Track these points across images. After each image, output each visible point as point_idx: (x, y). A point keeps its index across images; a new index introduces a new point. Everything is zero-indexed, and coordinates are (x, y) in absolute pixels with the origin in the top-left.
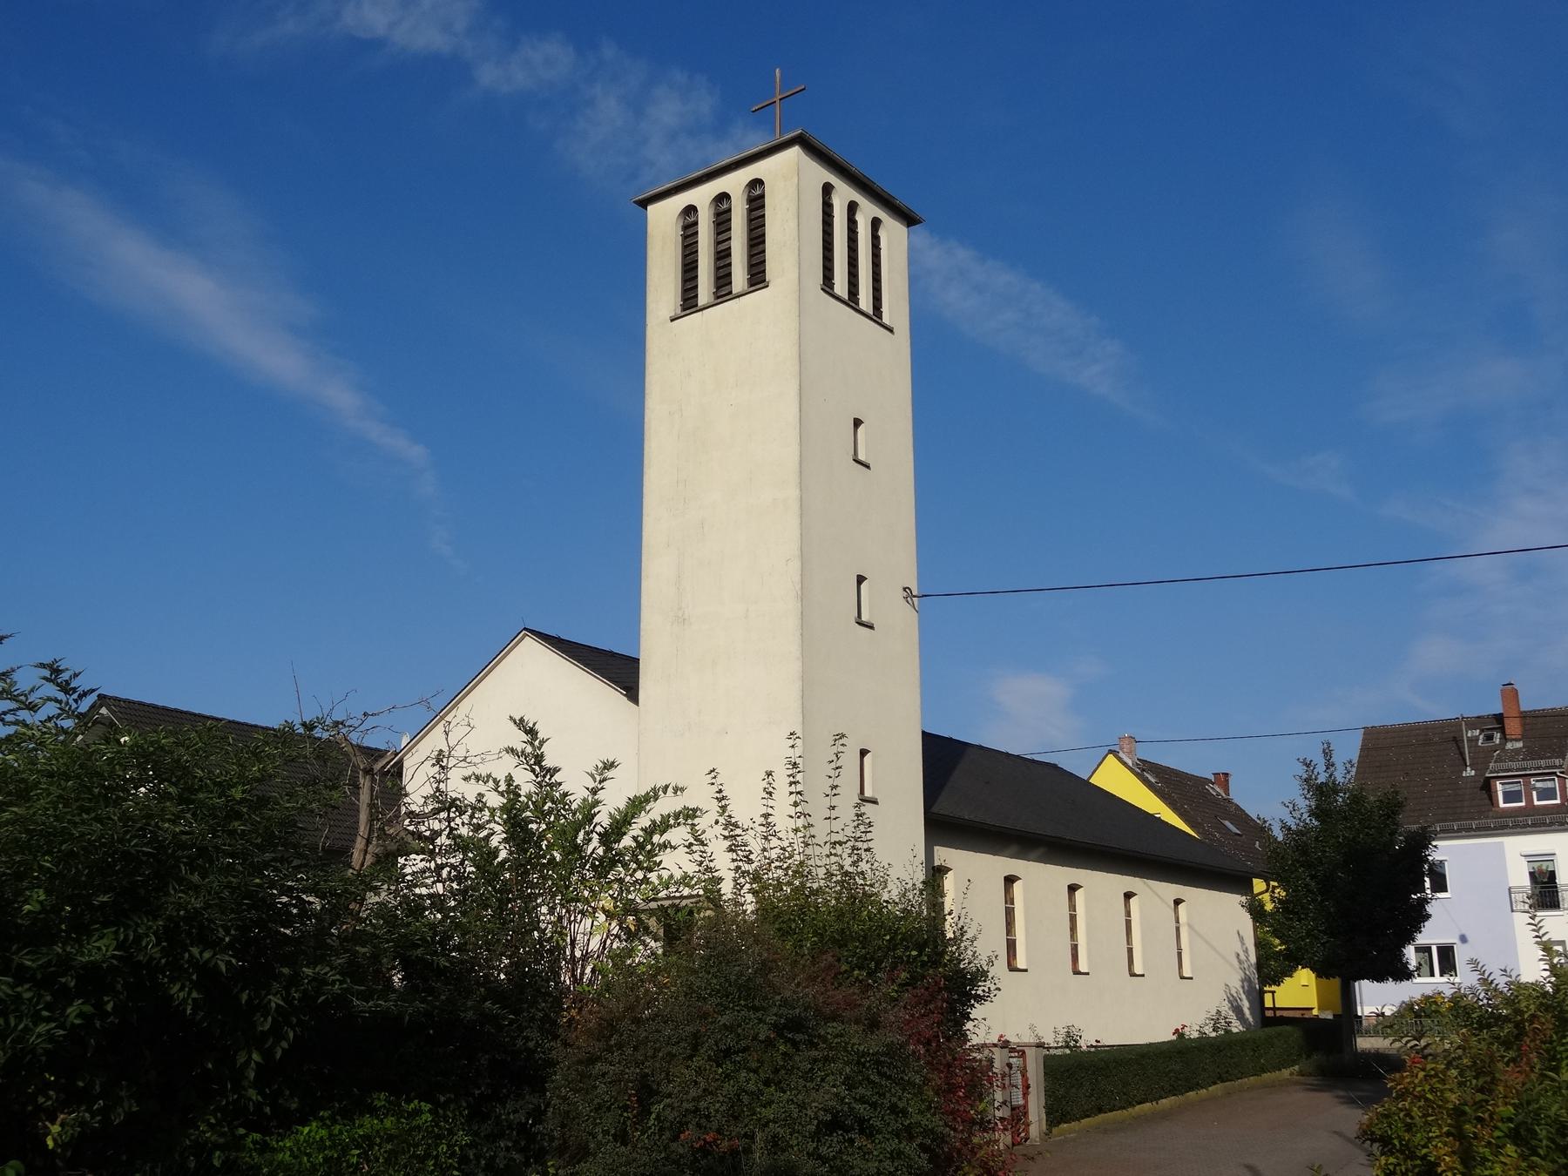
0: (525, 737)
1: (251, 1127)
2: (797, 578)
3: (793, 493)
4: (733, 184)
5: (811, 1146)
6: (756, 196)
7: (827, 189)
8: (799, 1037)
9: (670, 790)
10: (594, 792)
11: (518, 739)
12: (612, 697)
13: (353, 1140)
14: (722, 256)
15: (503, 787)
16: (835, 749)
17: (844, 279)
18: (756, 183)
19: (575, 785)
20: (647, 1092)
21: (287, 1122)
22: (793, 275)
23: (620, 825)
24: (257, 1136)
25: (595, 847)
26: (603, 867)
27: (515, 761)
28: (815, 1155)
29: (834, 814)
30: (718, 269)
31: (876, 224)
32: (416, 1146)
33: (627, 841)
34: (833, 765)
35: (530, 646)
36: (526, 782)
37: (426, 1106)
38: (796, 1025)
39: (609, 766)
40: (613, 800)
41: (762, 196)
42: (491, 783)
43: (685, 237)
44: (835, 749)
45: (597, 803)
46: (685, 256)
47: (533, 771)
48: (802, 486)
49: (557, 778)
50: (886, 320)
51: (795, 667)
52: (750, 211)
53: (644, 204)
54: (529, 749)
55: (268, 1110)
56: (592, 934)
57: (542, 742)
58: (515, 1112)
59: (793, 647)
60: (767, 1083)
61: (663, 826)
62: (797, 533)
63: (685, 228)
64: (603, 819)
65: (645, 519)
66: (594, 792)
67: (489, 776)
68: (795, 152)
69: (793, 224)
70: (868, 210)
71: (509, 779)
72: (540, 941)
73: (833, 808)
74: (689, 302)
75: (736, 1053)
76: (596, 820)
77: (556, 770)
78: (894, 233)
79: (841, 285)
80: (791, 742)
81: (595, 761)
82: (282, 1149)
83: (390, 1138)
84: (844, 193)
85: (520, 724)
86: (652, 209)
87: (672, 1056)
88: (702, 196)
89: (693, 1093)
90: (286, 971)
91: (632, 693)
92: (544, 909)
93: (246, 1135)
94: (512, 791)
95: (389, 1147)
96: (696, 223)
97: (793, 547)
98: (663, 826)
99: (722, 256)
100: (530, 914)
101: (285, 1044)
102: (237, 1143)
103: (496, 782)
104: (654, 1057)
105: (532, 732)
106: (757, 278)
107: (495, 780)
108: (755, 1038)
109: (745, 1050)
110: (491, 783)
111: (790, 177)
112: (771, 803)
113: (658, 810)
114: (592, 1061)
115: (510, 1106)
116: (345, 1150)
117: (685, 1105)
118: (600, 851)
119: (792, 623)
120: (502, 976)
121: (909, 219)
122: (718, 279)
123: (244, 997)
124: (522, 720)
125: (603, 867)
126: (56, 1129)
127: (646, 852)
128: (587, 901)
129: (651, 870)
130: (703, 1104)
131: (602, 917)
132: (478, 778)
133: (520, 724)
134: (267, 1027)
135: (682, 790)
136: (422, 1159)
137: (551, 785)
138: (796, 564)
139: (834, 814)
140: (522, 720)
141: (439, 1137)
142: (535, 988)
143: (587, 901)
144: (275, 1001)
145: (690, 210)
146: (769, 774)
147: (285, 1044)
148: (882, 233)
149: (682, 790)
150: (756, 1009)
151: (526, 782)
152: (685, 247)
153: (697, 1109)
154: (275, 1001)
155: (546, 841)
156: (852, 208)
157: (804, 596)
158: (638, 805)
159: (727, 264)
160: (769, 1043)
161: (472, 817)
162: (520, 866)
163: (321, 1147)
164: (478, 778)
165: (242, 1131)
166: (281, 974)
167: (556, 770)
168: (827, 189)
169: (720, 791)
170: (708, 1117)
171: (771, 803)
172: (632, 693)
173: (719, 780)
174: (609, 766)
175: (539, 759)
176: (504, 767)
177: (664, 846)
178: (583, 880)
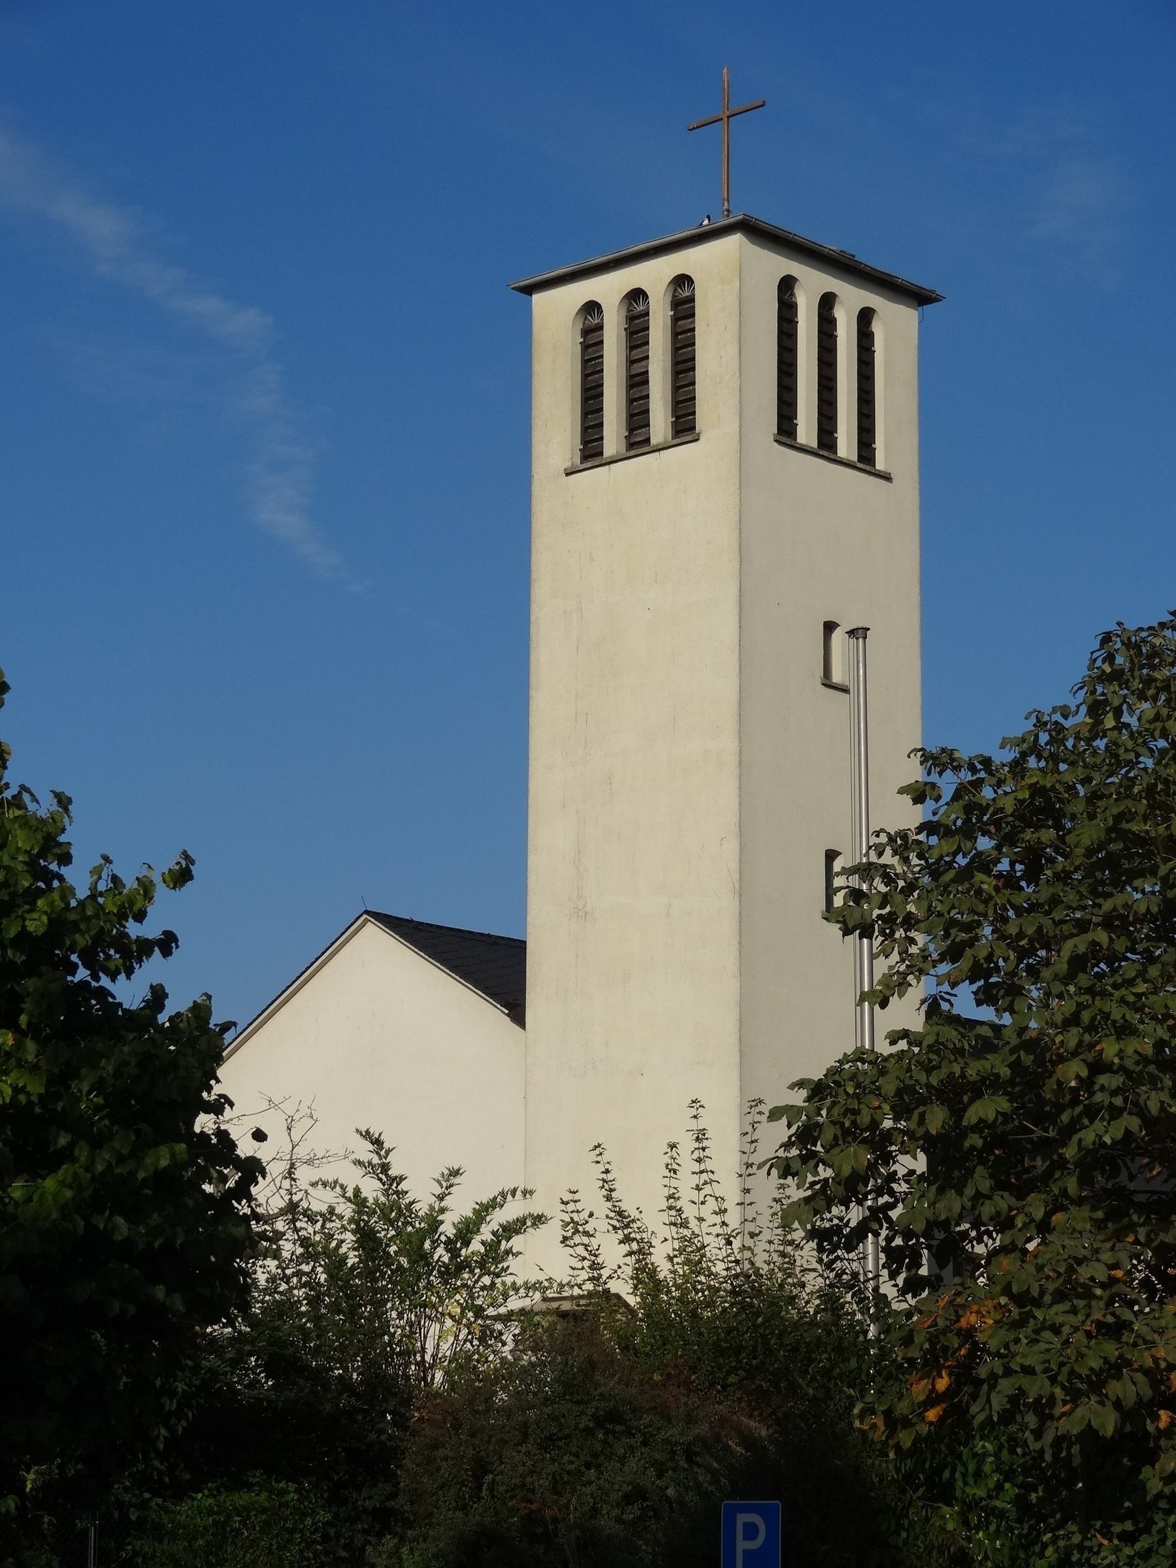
0: (371, 1147)
1: (156, 1494)
2: (734, 865)
3: (729, 744)
4: (653, 275)
5: (616, 1512)
6: (683, 306)
7: (787, 285)
8: (618, 1428)
9: (519, 1193)
10: (441, 1198)
11: (364, 1151)
12: (492, 1015)
13: (236, 1509)
14: (637, 382)
15: (350, 1194)
16: (749, 1118)
17: (817, 412)
18: (683, 281)
19: (420, 1192)
20: (480, 1468)
21: (180, 1492)
22: (731, 426)
23: (467, 1231)
24: (159, 1501)
25: (441, 1254)
26: (450, 1272)
27: (362, 1171)
28: (619, 1520)
29: (749, 1198)
30: (630, 401)
31: (865, 317)
32: (285, 1520)
33: (476, 1246)
34: (748, 1138)
35: (374, 936)
36: (372, 1189)
37: (292, 1487)
38: (614, 1416)
39: (456, 1173)
40: (460, 1207)
41: (691, 299)
42: (338, 1189)
43: (585, 347)
44: (749, 1118)
45: (443, 1211)
46: (585, 376)
47: (380, 1180)
48: (742, 734)
49: (403, 1186)
50: (880, 465)
51: (730, 988)
52: (675, 319)
53: (529, 290)
54: (376, 1160)
55: (167, 1480)
56: (440, 1339)
57: (388, 1152)
58: (370, 1498)
59: (729, 960)
60: (588, 1466)
61: (511, 1229)
62: (736, 801)
63: (586, 332)
64: (448, 1229)
65: (532, 764)
66: (441, 1198)
67: (336, 1182)
68: (735, 241)
69: (732, 350)
70: (852, 298)
71: (357, 1191)
72: (390, 1344)
73: (748, 1191)
74: (591, 451)
75: (560, 1439)
76: (441, 1229)
77: (402, 1179)
78: (897, 326)
79: (806, 429)
80: (693, 1112)
81: (441, 1168)
82: (179, 1513)
83: (264, 1511)
84: (812, 284)
85: (367, 1135)
86: (537, 298)
87: (504, 1442)
88: (609, 289)
89: (521, 1469)
90: (189, 1363)
91: (517, 1013)
92: (394, 1314)
93: (150, 1500)
94: (358, 1199)
95: (264, 1517)
96: (600, 327)
97: (729, 819)
98: (511, 1229)
99: (637, 382)
100: (379, 1318)
101: (184, 1423)
102: (144, 1505)
103: (343, 1188)
104: (489, 1442)
105: (378, 1143)
106: (685, 426)
107: (342, 1186)
108: (576, 1427)
109: (568, 1437)
110: (338, 1189)
111: (730, 277)
112: (674, 1183)
113: (498, 1218)
114: (435, 1447)
115: (365, 1492)
116: (229, 1518)
117: (514, 1481)
118: (446, 1259)
119: (727, 928)
120: (355, 1376)
121: (919, 297)
122: (631, 416)
123: (158, 1383)
124: (368, 1132)
125: (450, 1272)
126: (31, 1476)
127: (494, 1255)
128: (434, 1306)
129: (498, 1276)
130: (529, 1480)
131: (449, 1323)
132: (325, 1184)
133: (367, 1135)
134: (174, 1407)
135: (531, 1193)
136: (292, 1532)
137: (397, 1193)
138: (732, 846)
139: (749, 1198)
140: (368, 1132)
141: (304, 1515)
142: (388, 1385)
143: (434, 1306)
144: (181, 1387)
145: (592, 308)
146: (673, 1146)
147: (1031, 961)
148: (877, 328)
149: (531, 1193)
150: (579, 1403)
151: (372, 1189)
152: (585, 362)
153: (524, 1485)
154: (181, 1387)
155: (400, 1250)
156: (827, 302)
157: (743, 890)
158: (484, 1210)
159: (641, 398)
160: (589, 1432)
161: (323, 1226)
162: (370, 1275)
163: (210, 1512)
164: (325, 1184)
165: (147, 1495)
166: (187, 1365)
167: (402, 1179)
168: (787, 285)
169: (607, 1171)
170: (533, 1491)
171: (674, 1183)
172: (517, 1013)
173: (605, 1158)
174: (456, 1173)
175: (385, 1168)
176: (354, 1178)
177: (508, 1252)
178: (430, 1286)
